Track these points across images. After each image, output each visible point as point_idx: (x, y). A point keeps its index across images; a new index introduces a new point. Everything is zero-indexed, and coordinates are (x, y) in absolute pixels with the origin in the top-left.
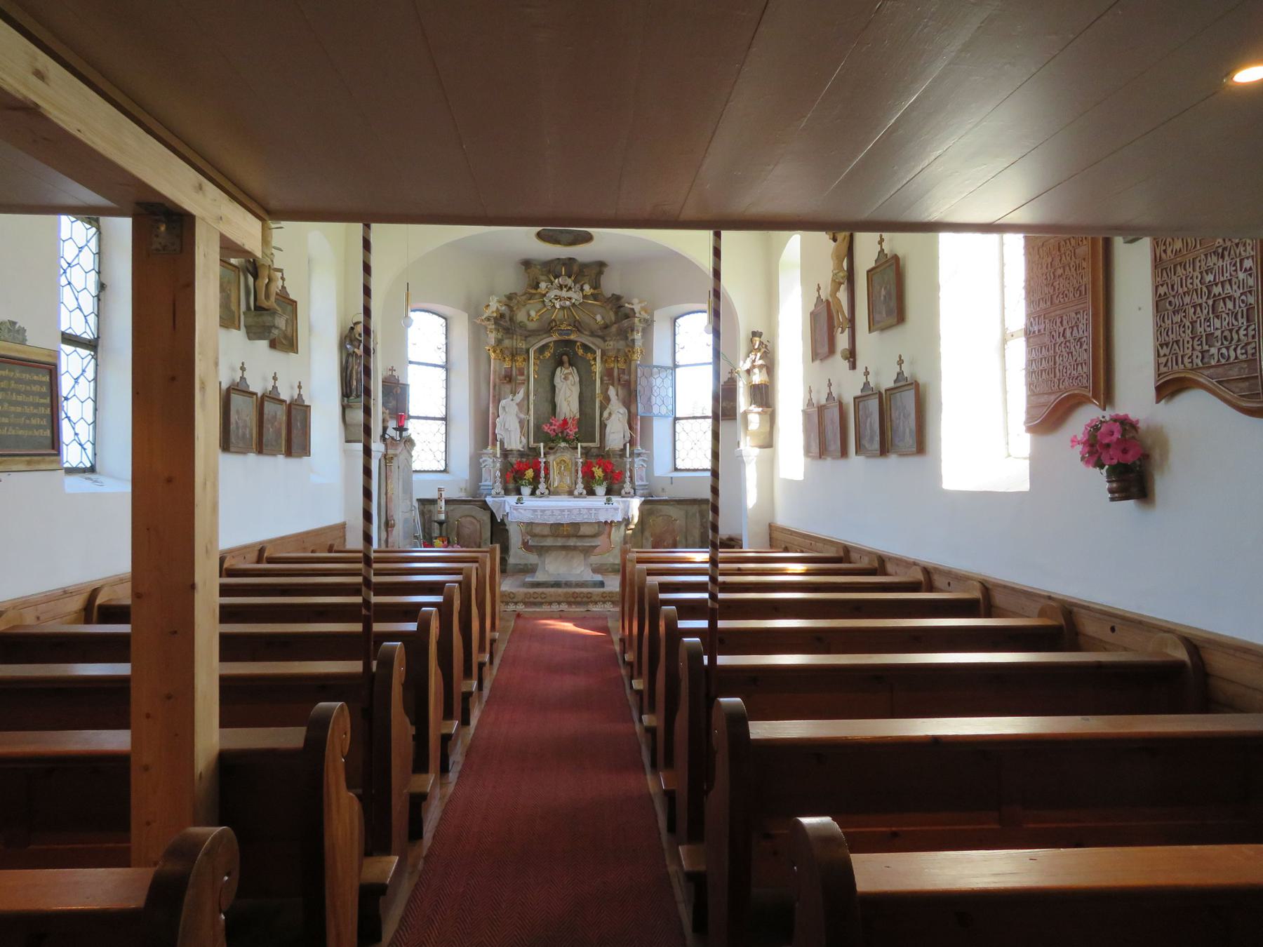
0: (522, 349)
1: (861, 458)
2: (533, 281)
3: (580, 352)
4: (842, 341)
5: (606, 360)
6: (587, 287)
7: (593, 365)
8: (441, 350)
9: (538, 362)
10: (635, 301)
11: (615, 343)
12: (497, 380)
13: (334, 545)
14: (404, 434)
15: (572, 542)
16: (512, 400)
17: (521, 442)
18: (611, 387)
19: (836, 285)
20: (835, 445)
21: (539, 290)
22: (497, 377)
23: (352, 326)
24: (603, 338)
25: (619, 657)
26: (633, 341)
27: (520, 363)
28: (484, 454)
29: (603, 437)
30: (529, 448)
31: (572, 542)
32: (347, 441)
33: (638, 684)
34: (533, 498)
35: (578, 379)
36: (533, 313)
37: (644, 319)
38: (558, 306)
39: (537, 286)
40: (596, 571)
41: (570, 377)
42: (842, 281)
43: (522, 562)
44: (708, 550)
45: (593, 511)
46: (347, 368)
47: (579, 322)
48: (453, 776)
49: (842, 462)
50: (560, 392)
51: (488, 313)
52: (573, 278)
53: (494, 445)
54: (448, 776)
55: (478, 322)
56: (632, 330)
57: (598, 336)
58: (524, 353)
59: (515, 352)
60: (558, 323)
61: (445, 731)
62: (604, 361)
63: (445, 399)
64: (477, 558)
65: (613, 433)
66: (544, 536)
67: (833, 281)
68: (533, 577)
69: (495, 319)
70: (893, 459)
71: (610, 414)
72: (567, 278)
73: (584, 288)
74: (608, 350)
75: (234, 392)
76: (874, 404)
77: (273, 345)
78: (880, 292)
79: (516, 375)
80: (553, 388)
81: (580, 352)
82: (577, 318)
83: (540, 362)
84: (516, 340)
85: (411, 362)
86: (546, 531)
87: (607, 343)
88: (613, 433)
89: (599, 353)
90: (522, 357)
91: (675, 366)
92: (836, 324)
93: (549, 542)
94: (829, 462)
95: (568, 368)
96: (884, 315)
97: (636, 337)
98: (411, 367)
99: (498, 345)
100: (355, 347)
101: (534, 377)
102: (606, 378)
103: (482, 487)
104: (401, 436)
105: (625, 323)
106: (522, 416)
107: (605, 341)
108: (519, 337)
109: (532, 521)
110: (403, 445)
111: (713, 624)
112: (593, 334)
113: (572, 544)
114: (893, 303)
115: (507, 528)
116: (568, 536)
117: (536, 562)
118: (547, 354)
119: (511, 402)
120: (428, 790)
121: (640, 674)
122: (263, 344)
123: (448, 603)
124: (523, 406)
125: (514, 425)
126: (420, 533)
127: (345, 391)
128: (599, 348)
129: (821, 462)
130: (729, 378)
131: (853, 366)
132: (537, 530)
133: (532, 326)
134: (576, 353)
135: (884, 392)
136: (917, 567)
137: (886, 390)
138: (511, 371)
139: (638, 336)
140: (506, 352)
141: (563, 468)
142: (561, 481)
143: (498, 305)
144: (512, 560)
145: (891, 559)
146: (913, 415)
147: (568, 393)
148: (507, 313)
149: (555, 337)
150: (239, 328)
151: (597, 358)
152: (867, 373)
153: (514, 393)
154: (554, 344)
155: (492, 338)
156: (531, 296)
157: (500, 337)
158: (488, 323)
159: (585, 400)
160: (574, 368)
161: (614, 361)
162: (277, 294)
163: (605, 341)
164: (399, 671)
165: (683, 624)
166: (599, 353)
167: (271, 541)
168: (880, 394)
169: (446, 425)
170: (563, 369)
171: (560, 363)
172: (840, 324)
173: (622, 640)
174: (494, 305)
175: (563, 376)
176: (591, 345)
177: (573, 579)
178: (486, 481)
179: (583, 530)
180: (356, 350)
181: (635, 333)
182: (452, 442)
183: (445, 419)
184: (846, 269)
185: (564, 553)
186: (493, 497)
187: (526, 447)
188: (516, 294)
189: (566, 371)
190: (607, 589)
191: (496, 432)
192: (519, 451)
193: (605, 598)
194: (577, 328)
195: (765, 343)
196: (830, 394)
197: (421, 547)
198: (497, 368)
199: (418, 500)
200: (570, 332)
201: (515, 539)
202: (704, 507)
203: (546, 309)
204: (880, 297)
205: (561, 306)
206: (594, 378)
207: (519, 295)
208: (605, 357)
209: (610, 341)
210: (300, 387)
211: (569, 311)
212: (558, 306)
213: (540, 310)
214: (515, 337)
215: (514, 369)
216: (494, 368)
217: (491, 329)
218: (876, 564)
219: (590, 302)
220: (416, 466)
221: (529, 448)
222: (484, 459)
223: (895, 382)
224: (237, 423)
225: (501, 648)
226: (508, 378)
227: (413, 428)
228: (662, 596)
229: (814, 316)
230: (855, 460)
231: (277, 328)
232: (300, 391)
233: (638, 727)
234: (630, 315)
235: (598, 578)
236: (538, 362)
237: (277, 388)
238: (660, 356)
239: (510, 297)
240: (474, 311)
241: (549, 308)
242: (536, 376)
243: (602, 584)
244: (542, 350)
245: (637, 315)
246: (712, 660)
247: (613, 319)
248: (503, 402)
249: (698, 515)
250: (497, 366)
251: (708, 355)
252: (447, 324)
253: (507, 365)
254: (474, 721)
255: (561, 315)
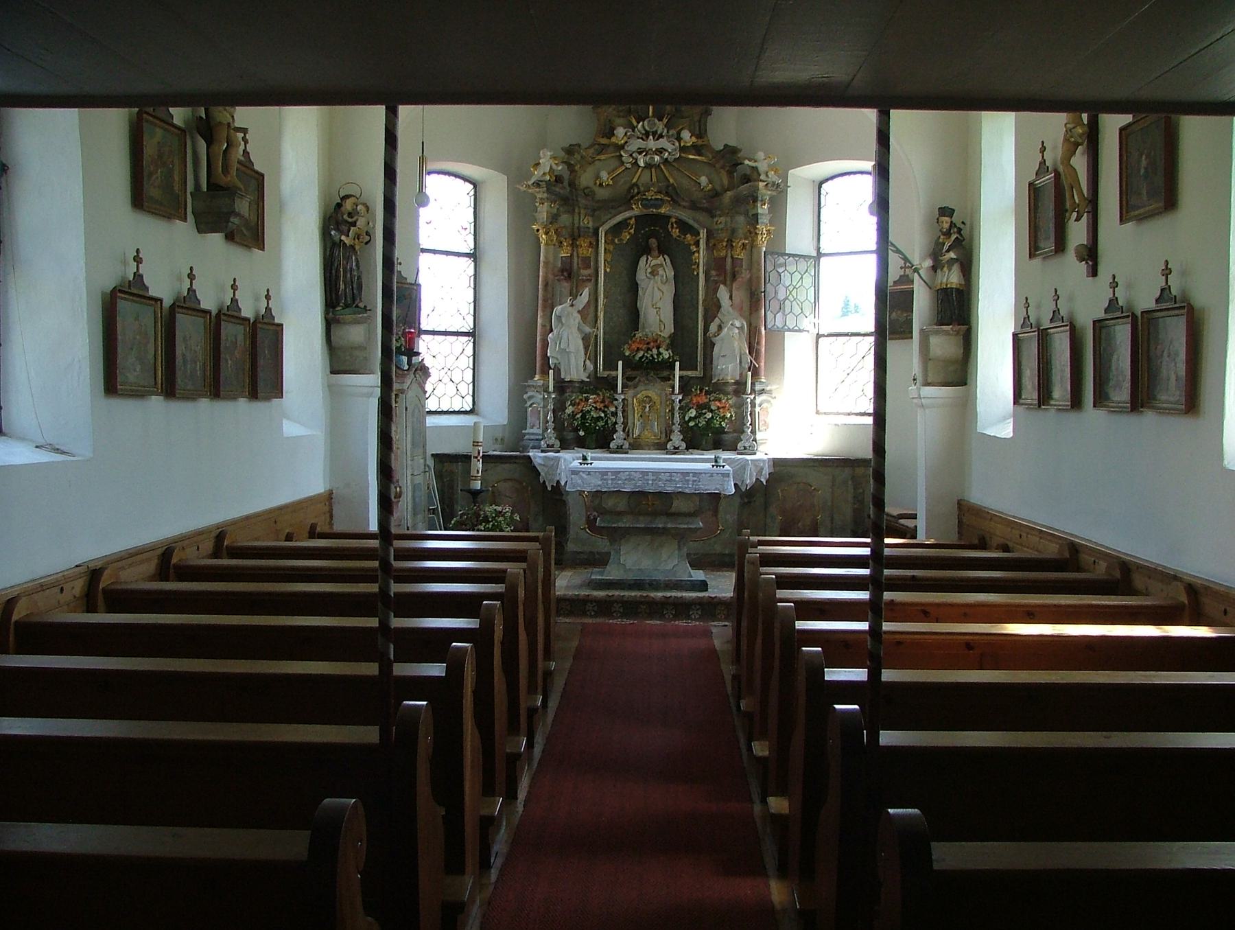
0: (589, 228)
1: (1100, 414)
2: (605, 126)
3: (675, 232)
4: (1077, 232)
5: (715, 245)
6: (686, 135)
8: (468, 231)
9: (611, 247)
10: (761, 155)
12: (551, 276)
13: (316, 524)
14: (414, 360)
15: (659, 523)
16: (572, 305)
19: (1071, 147)
20: (1060, 391)
21: (613, 140)
23: (339, 201)
24: (711, 213)
25: (732, 700)
26: (756, 216)
27: (585, 250)
28: (529, 386)
29: (708, 361)
30: (596, 377)
31: (659, 523)
32: (332, 372)
33: (760, 749)
36: (604, 175)
37: (774, 183)
38: (642, 164)
39: (611, 133)
40: (696, 565)
41: (661, 272)
42: (1080, 141)
43: (587, 549)
44: (868, 540)
45: (691, 478)
46: (332, 264)
47: (674, 188)
48: (494, 874)
49: (1073, 416)
51: (537, 174)
52: (665, 121)
53: (545, 373)
54: (490, 871)
55: (523, 188)
56: (755, 200)
59: (576, 234)
60: (642, 189)
61: (485, 812)
62: (710, 248)
63: (472, 305)
64: (525, 551)
66: (620, 514)
67: (1066, 140)
68: (601, 573)
69: (548, 183)
70: (1149, 418)
71: (720, 328)
72: (656, 121)
73: (682, 135)
75: (180, 310)
76: (1122, 334)
77: (230, 237)
78: (1139, 161)
80: (634, 288)
81: (675, 232)
82: (671, 181)
83: (614, 249)
84: (579, 213)
85: (423, 251)
86: (622, 505)
87: (715, 220)
89: (703, 234)
90: (587, 241)
91: (820, 255)
92: (1068, 205)
93: (625, 523)
94: (1049, 416)
96: (1145, 198)
97: (760, 211)
98: (424, 259)
99: (551, 223)
100: (342, 233)
101: (605, 271)
102: (713, 273)
103: (527, 437)
104: (409, 363)
105: (744, 189)
106: (588, 329)
109: (599, 489)
110: (413, 376)
111: (874, 674)
112: (694, 206)
113: (660, 526)
114: (1159, 180)
115: (564, 498)
116: (655, 514)
117: (606, 550)
118: (626, 236)
120: (466, 899)
121: (763, 735)
122: (217, 238)
123: (487, 627)
124: (589, 314)
125: (576, 345)
126: (437, 504)
127: (329, 298)
129: (1040, 414)
130: (901, 276)
131: (1094, 272)
132: (610, 503)
133: (602, 194)
134: (669, 234)
135: (1139, 314)
136: (1179, 584)
137: (1142, 312)
138: (571, 263)
139: (763, 209)
141: (647, 409)
142: (643, 428)
143: (552, 162)
144: (571, 547)
145: (1140, 567)
146: (1182, 356)
147: (658, 294)
148: (566, 175)
149: (637, 210)
150: (185, 220)
151: (701, 241)
152: (1114, 285)
153: (574, 295)
155: (543, 212)
156: (603, 149)
158: (537, 190)
159: (683, 305)
160: (666, 256)
162: (239, 162)
163: (713, 216)
164: (426, 740)
165: (835, 675)
166: (703, 234)
167: (234, 523)
168: (1134, 316)
169: (474, 343)
170: (650, 258)
171: (647, 251)
172: (1075, 206)
173: (736, 678)
174: (547, 163)
175: (649, 270)
176: (691, 222)
177: (660, 577)
178: (532, 427)
179: (679, 505)
180: (343, 238)
181: (759, 205)
182: (484, 370)
183: (472, 334)
184: (1086, 123)
185: (648, 538)
186: (542, 451)
187: (592, 377)
188: (579, 145)
190: (711, 593)
192: (582, 382)
193: (711, 608)
194: (671, 197)
195: (958, 226)
196: (1056, 312)
197: (441, 530)
198: (551, 259)
199: (433, 455)
200: (660, 202)
201: (576, 516)
202: (860, 471)
203: (624, 168)
204: (1139, 171)
205: (645, 162)
207: (583, 146)
208: (712, 242)
210: (268, 297)
211: (658, 170)
212: (642, 164)
213: (613, 171)
215: (576, 258)
216: (546, 257)
217: (541, 199)
218: (1117, 574)
219: (691, 157)
220: (432, 405)
221: (596, 377)
222: (530, 394)
223: (1157, 301)
224: (184, 355)
225: (559, 683)
226: (567, 272)
227: (427, 348)
228: (801, 625)
229: (1034, 192)
230: (1091, 415)
231: (238, 215)
232: (268, 303)
233: (757, 808)
234: (751, 177)
235: (699, 575)
236: (611, 247)
237: (237, 301)
238: (797, 238)
239: (570, 151)
240: (516, 174)
241: (629, 166)
243: (703, 586)
244: (617, 229)
245: (762, 177)
246: (874, 737)
247: (726, 182)
248: (558, 309)
249: (850, 482)
250: (549, 253)
251: (870, 239)
252: (475, 192)
253: (564, 253)
254: (522, 794)
255: (646, 177)
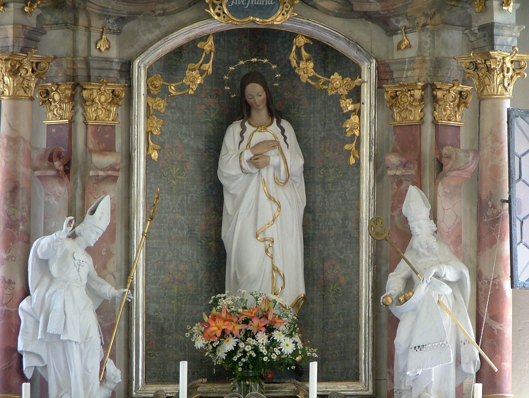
5: (395, 97)
7: (348, 116)
9: (161, 104)
11: (426, 37)
16: (73, 236)
17: (103, 380)
18: (413, 192)
22: (22, 159)
34: (400, 52)
35: (301, 162)
41: (274, 158)
50: (237, 208)
57: (367, 16)
58: (114, 74)
65: (420, 347)
74: (402, 62)
79: (88, 151)
84: (88, 29)
87: (397, 39)
88: (420, 347)
95: (264, 127)
97: (498, 18)
99: (24, 50)
101: (148, 158)
102: (393, 159)
107: (391, 32)
108: (97, 23)
119: (69, 244)
128: (369, 56)
140: (53, 69)
154: (215, 41)
157: (32, 21)
160: (285, 124)
161: (422, 99)
163: (391, 32)
170: (250, 129)
175: (248, 155)
176: (341, 46)
189: (259, 137)
191: (20, 348)
206: (352, 161)
209: (407, 30)
214: (82, 21)
242: (155, 155)
